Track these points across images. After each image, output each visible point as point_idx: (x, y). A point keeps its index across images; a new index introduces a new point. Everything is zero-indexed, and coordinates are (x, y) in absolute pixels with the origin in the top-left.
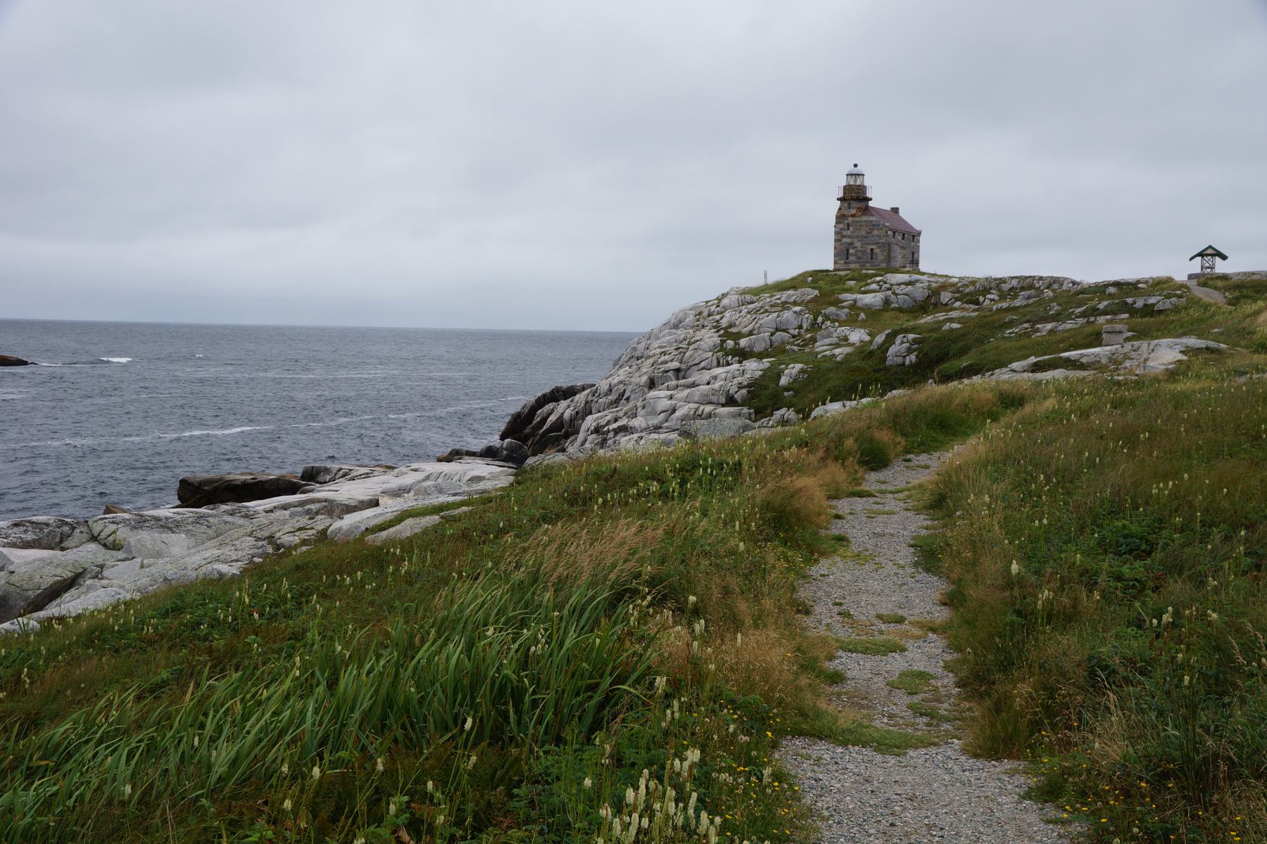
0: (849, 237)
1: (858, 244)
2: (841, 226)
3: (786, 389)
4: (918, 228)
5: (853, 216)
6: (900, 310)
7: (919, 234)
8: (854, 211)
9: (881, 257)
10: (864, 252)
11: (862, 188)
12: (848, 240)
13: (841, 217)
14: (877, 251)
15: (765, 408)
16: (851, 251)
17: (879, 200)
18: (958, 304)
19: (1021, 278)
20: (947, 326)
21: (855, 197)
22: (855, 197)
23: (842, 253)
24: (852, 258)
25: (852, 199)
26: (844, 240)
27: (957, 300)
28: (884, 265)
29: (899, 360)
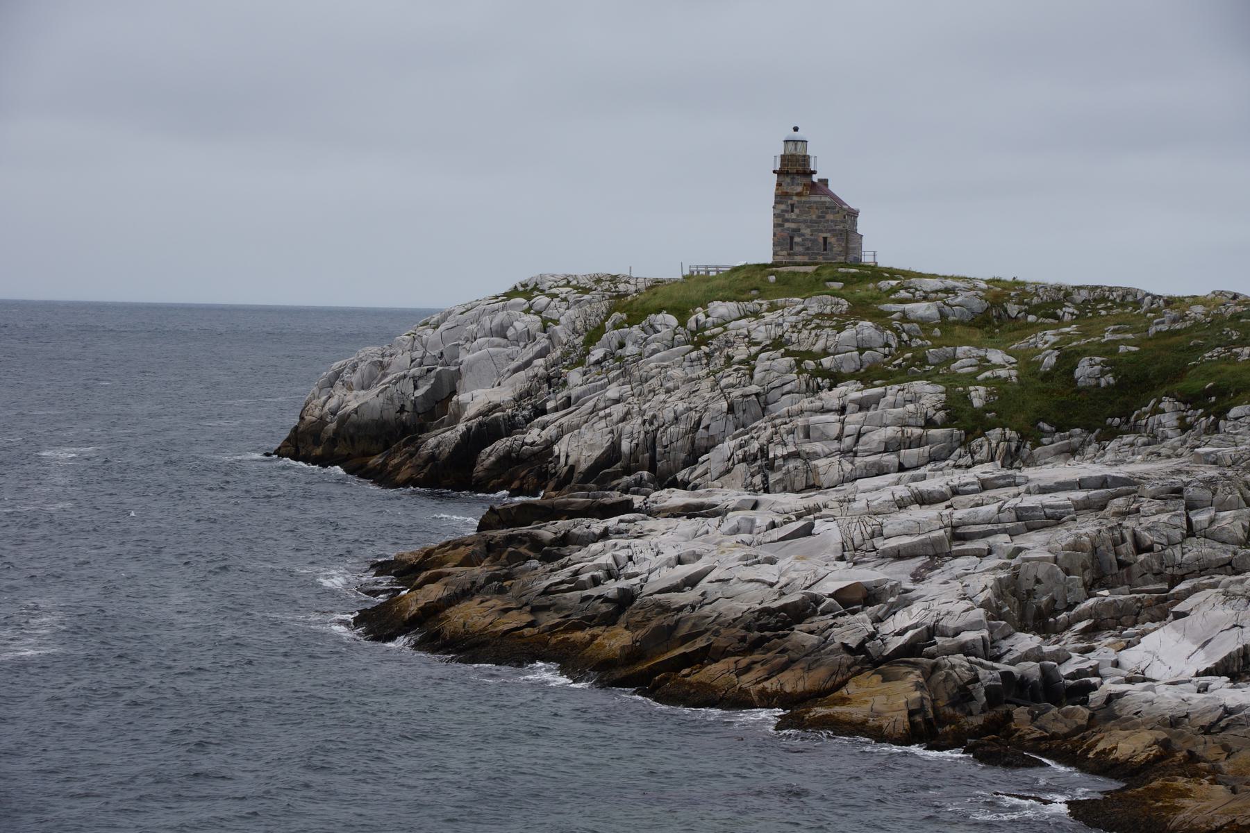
0: (793, 221)
1: (807, 231)
2: (783, 207)
3: (985, 410)
4: (851, 202)
5: (799, 194)
6: (960, 323)
7: (854, 214)
8: (799, 189)
9: (837, 249)
10: (814, 241)
11: (806, 159)
12: (793, 226)
13: (781, 197)
14: (832, 240)
15: (975, 428)
16: (797, 239)
17: (821, 169)
18: (1031, 318)
19: (1128, 292)
20: (1122, 348)
21: (794, 168)
22: (794, 168)
23: (784, 240)
24: (797, 249)
25: (798, 173)
26: (787, 225)
27: (1028, 313)
28: (842, 259)
29: (1093, 382)
